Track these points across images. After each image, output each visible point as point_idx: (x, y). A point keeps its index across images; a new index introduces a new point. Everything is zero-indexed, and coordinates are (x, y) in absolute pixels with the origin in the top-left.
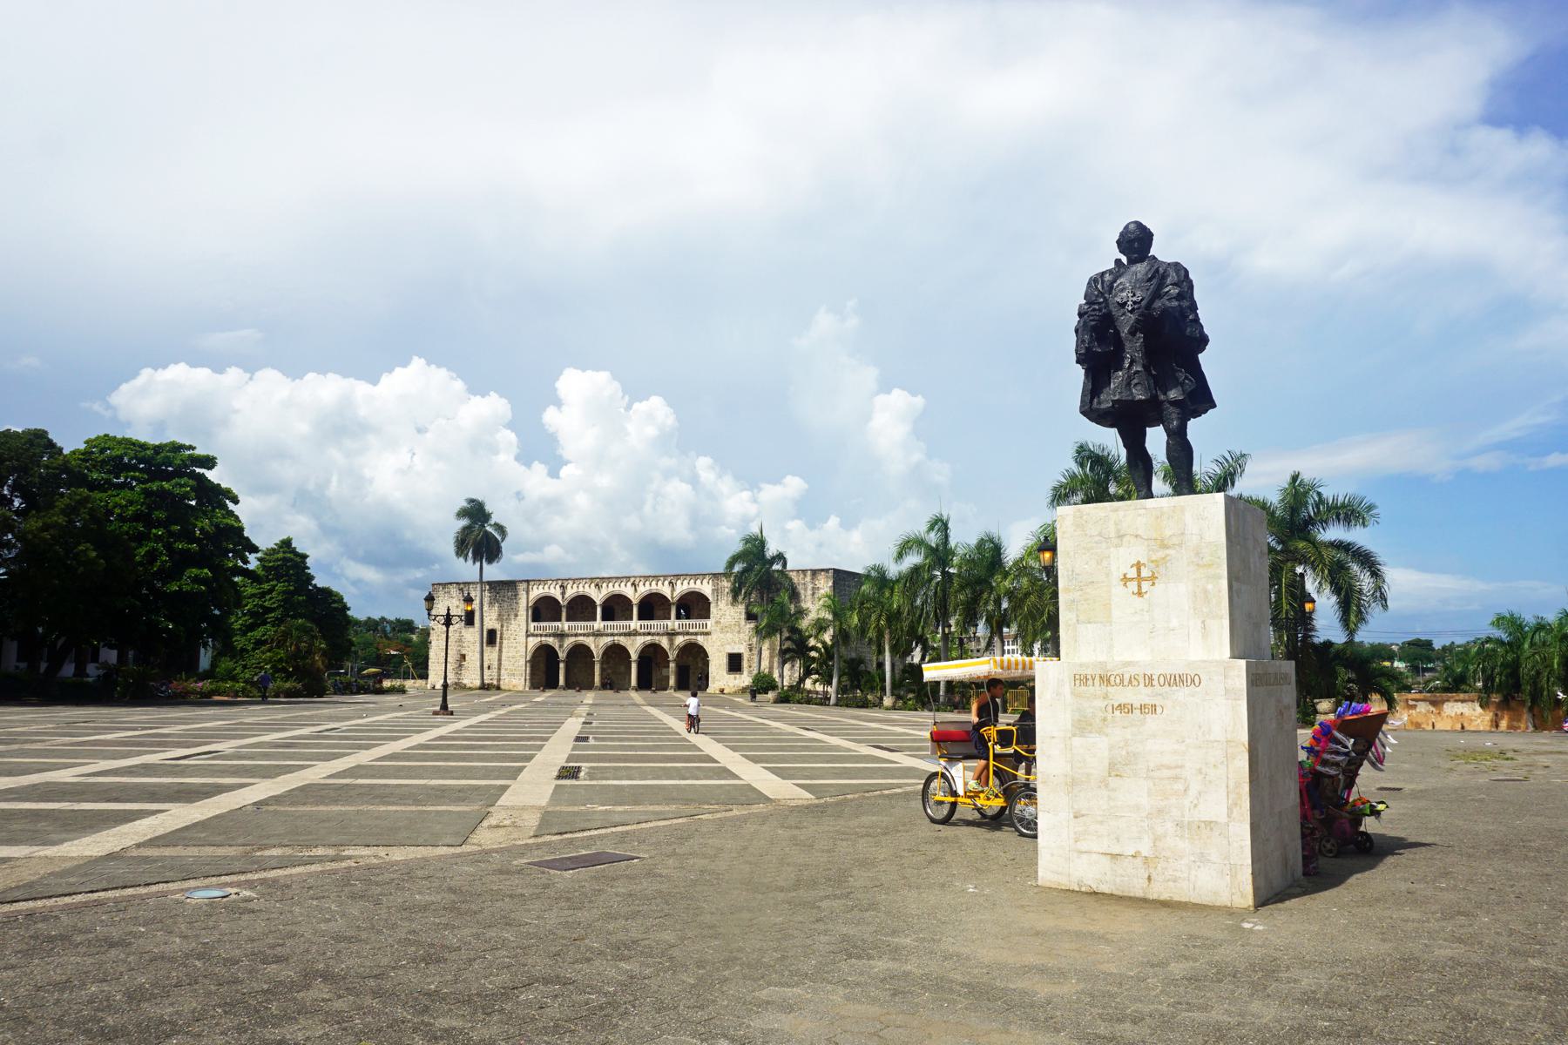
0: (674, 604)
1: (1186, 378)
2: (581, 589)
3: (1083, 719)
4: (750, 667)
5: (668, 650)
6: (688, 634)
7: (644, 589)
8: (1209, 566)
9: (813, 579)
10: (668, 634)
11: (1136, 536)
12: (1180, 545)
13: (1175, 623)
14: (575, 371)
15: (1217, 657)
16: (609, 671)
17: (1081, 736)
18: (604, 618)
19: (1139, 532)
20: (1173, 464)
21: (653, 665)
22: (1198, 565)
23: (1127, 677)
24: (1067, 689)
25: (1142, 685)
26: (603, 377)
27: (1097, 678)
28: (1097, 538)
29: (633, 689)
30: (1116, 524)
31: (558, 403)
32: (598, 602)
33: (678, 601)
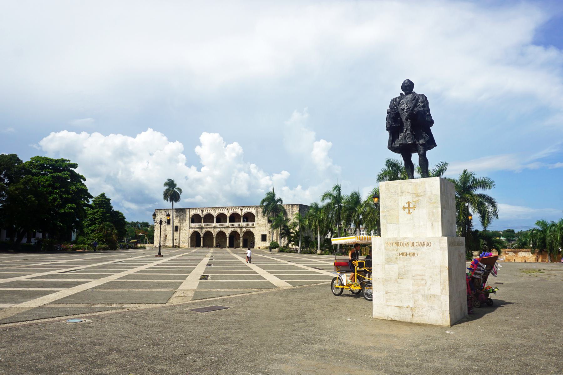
0: (242, 217)
1: (426, 136)
2: (209, 211)
3: (389, 258)
4: (269, 239)
5: (240, 233)
6: (247, 227)
7: (231, 211)
8: (434, 203)
9: (292, 208)
10: (240, 228)
11: (408, 192)
12: (424, 196)
13: (422, 223)
14: (207, 133)
15: (437, 236)
16: (219, 241)
18: (217, 222)
19: (409, 191)
20: (421, 166)
21: (235, 239)
22: (430, 203)
23: (405, 243)
25: (410, 246)
26: (216, 135)
27: (394, 243)
28: (394, 193)
29: (227, 247)
30: (401, 188)
31: (200, 145)
32: (215, 216)
33: (244, 216)
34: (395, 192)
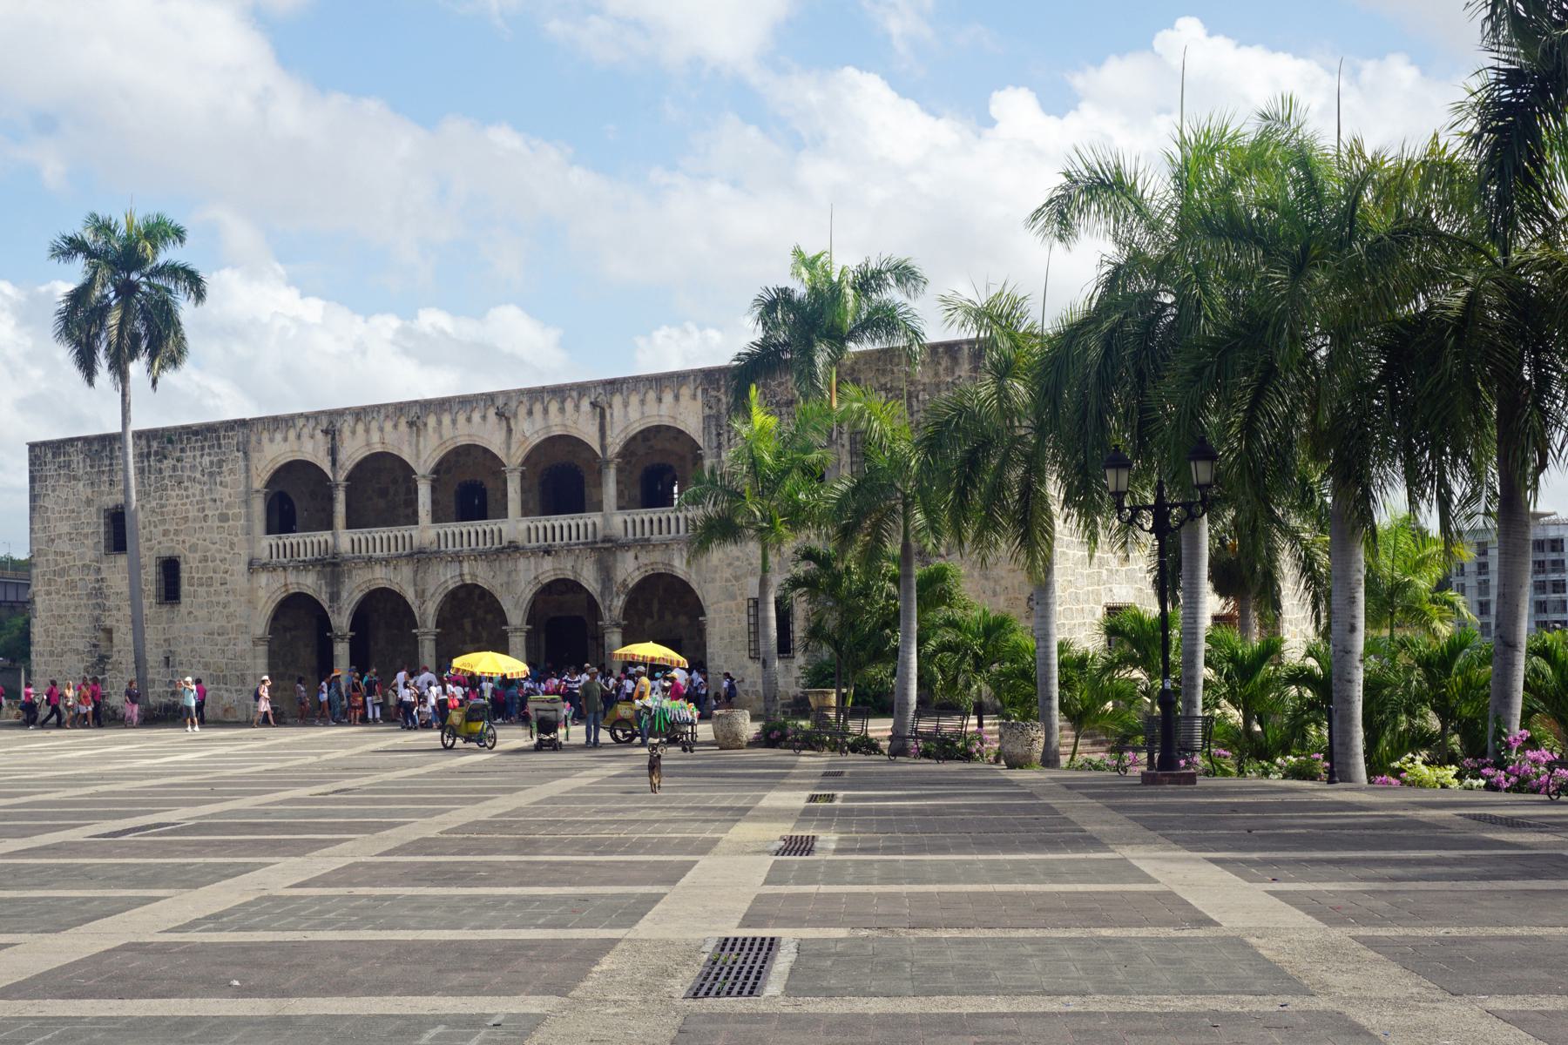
2: (375, 437)
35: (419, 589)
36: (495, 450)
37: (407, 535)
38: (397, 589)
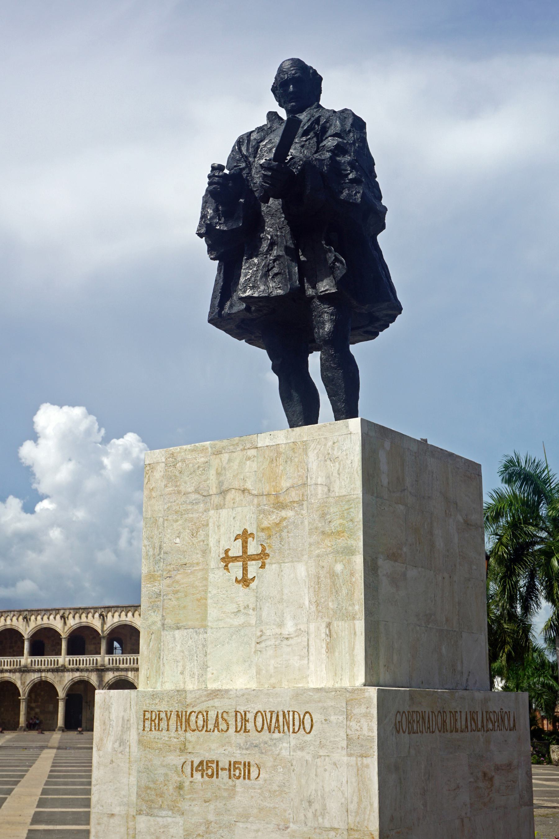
0: (104, 637)
1: (337, 260)
2: (9, 622)
3: (152, 785)
6: (118, 669)
7: (73, 622)
8: (338, 533)
10: (97, 670)
11: (243, 491)
12: (300, 503)
13: (289, 628)
14: (52, 407)
15: (346, 684)
16: (37, 710)
17: (147, 814)
18: (33, 653)
19: (249, 485)
20: (328, 388)
21: (84, 704)
22: (323, 533)
23: (212, 715)
24: (133, 736)
25: (232, 729)
26: (78, 412)
27: (174, 717)
28: (193, 496)
29: (59, 730)
30: (218, 474)
31: (35, 437)
32: (26, 636)
33: (108, 634)
34: (197, 491)
35: (23, 681)
36: (58, 630)
37: (18, 660)
38: (13, 681)
